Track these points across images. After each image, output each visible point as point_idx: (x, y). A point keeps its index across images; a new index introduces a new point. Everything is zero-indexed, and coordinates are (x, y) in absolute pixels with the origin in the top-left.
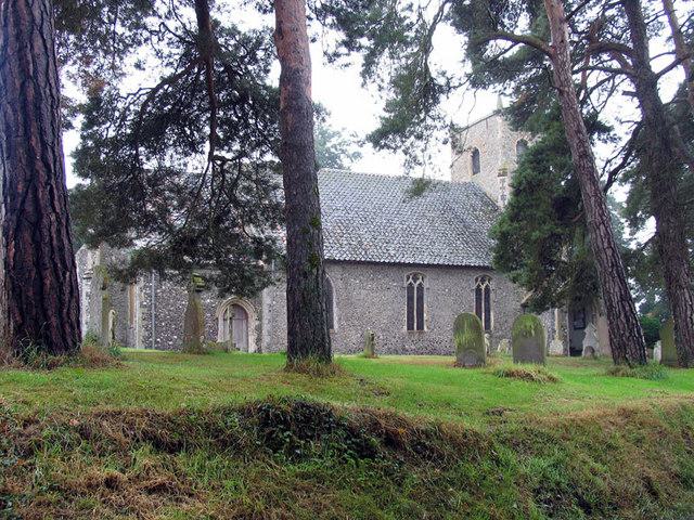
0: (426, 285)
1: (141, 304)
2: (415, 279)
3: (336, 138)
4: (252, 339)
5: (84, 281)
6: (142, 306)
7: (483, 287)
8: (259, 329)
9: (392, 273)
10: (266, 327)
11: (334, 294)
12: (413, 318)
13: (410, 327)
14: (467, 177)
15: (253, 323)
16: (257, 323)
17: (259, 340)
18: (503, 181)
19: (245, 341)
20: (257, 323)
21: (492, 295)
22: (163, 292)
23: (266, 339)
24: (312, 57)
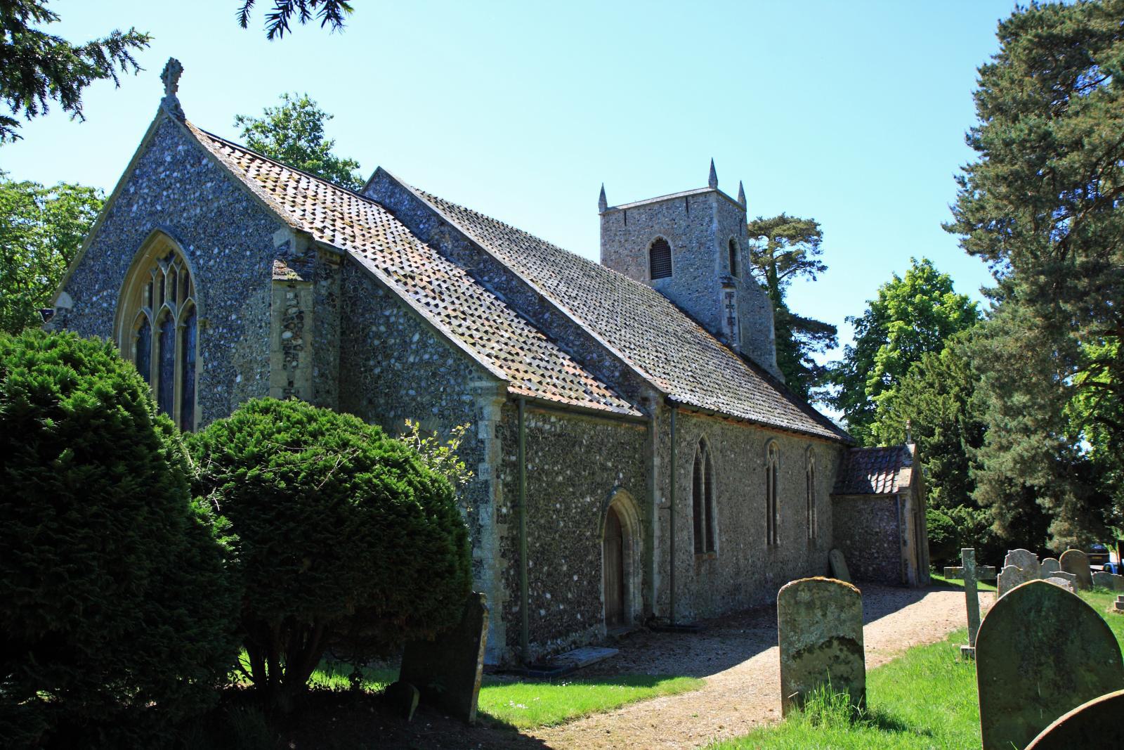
6: (501, 519)
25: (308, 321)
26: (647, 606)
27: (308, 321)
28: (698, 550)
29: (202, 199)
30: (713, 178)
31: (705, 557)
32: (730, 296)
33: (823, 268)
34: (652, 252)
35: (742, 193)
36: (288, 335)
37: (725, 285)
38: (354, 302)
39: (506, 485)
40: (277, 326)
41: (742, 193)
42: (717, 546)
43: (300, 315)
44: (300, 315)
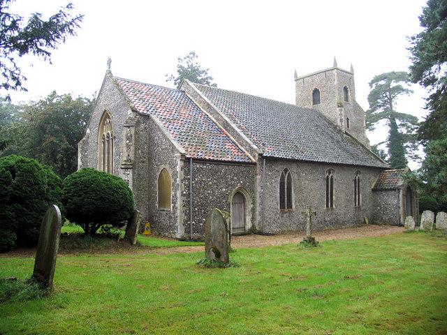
0: (335, 177)
1: (182, 192)
2: (330, 173)
3: (204, 74)
4: (248, 218)
5: (122, 170)
6: (183, 195)
7: (357, 177)
8: (253, 210)
9: (320, 168)
10: (258, 209)
11: (292, 183)
12: (284, 201)
13: (327, 206)
14: (310, 106)
15: (250, 206)
16: (252, 206)
17: (253, 219)
18: (341, 110)
19: (243, 220)
20: (252, 206)
21: (361, 183)
22: (196, 183)
23: (258, 218)
24: (361, 106)
25: (133, 137)
26: (253, 226)
27: (133, 137)
28: (282, 206)
29: (114, 100)
30: (335, 64)
31: (286, 210)
32: (341, 110)
33: (412, 92)
34: (313, 94)
35: (352, 67)
36: (128, 142)
37: (339, 107)
38: (151, 130)
39: (185, 185)
40: (125, 139)
41: (352, 67)
42: (294, 207)
43: (131, 136)
44: (131, 136)
